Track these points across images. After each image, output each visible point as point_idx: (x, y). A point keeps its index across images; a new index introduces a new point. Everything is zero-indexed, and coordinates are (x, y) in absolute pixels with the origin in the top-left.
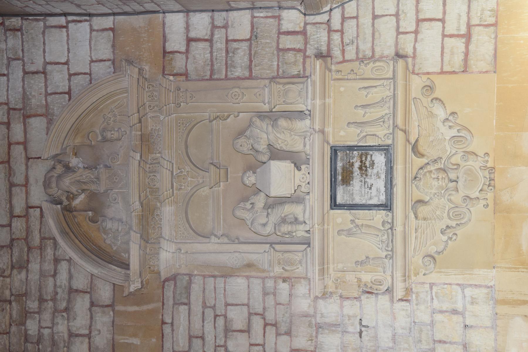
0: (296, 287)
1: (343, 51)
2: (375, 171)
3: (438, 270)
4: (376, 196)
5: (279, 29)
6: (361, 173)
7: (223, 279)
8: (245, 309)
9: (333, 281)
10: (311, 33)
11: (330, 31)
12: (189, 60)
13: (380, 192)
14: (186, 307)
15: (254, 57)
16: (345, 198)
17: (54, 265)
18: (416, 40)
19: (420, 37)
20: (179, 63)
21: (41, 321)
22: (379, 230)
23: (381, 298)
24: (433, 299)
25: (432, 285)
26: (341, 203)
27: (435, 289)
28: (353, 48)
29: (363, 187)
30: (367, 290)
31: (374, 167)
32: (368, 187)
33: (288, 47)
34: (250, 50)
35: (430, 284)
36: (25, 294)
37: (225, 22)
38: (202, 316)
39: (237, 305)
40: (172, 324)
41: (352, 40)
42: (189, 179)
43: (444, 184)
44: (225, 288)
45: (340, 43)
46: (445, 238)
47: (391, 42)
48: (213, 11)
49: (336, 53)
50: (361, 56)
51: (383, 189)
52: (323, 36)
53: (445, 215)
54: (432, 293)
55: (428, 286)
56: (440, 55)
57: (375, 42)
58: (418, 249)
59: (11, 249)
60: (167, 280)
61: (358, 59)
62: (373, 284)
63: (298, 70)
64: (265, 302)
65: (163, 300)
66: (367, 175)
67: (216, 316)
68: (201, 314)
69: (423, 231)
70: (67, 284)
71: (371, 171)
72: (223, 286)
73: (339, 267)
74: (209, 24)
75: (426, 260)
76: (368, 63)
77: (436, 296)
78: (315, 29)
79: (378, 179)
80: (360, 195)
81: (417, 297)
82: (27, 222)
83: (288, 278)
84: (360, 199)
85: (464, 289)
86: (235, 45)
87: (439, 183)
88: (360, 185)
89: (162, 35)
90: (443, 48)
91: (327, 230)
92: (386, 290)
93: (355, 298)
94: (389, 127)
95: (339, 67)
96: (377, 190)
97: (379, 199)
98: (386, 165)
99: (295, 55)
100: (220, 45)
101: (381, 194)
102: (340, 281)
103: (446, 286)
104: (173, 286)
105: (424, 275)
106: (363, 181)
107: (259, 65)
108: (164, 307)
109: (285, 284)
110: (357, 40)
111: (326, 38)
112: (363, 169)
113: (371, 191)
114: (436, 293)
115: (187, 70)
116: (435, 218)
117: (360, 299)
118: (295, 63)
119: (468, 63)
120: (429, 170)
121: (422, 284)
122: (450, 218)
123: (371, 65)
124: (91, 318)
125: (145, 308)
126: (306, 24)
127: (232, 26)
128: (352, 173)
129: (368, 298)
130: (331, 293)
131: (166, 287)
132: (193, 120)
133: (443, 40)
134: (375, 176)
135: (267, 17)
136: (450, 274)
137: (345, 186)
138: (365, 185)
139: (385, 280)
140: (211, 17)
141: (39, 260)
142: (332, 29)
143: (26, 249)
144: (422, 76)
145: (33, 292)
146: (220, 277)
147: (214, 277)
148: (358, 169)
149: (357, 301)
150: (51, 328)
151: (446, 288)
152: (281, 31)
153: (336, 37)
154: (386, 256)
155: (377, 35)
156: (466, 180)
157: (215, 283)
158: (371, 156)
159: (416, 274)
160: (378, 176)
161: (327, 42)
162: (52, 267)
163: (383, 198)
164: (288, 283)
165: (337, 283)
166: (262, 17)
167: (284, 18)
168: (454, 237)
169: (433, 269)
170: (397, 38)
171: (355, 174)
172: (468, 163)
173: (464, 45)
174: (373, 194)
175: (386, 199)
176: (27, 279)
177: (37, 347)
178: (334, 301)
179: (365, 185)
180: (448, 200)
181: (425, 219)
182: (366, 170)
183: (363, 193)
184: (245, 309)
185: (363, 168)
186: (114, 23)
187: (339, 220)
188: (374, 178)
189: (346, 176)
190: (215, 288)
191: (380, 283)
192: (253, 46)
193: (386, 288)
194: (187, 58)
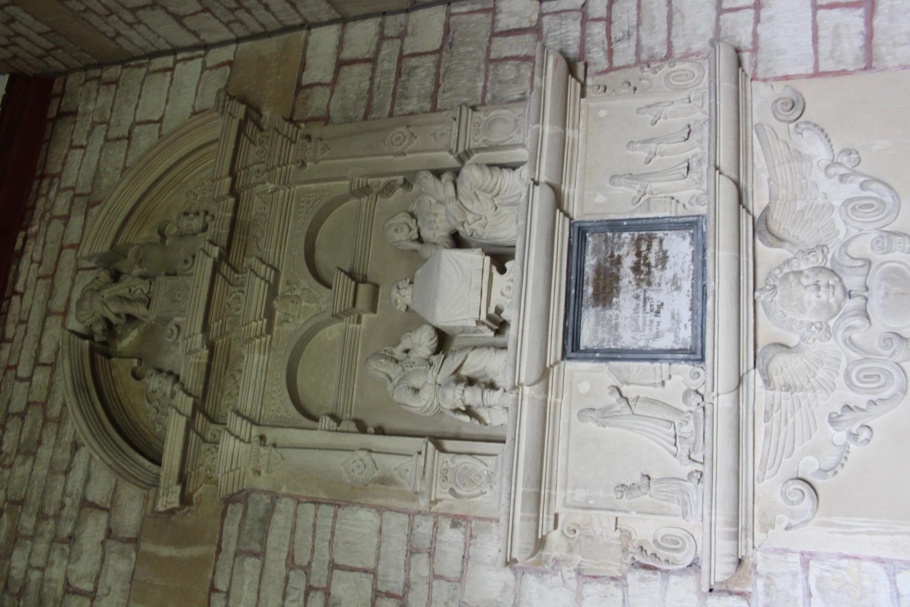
0: (478, 540)
1: (610, 53)
2: (669, 274)
3: (825, 519)
4: (670, 330)
5: (493, 28)
6: (637, 280)
7: (331, 510)
8: (366, 581)
9: (562, 532)
10: (550, 28)
11: (585, 20)
12: (335, 95)
13: (678, 322)
14: (258, 562)
15: (443, 78)
16: (600, 335)
17: (71, 453)
18: (757, 20)
19: (764, 14)
20: (318, 101)
21: (33, 554)
22: (678, 411)
23: (676, 583)
24: (810, 595)
25: (807, 559)
26: (590, 346)
27: (815, 569)
28: (629, 46)
29: (641, 310)
30: (644, 561)
31: (668, 265)
32: (652, 311)
33: (504, 55)
34: (438, 67)
35: (802, 554)
36: (22, 502)
37: (402, 29)
38: (284, 585)
39: (352, 570)
40: (228, 593)
41: (629, 32)
42: (304, 304)
43: (832, 300)
44: (333, 528)
45: (605, 38)
46: (840, 436)
47: (706, 29)
48: (384, 14)
49: (595, 56)
50: (644, 56)
51: (686, 315)
52: (572, 30)
53: (840, 380)
54: (807, 579)
55: (797, 558)
56: (811, 43)
57: (673, 31)
58: (770, 461)
59: (23, 419)
60: (230, 500)
61: (638, 62)
62: (659, 546)
63: (521, 92)
64: (410, 570)
65: (220, 540)
66: (649, 284)
67: (309, 589)
68: (283, 579)
69: (783, 417)
70: (81, 490)
71: (661, 274)
72: (330, 524)
73: (577, 498)
74: (376, 35)
75: (791, 488)
76: (660, 68)
77: (818, 588)
78: (557, 21)
79: (675, 293)
80: (633, 328)
81: (767, 587)
82: (52, 374)
83: (464, 517)
84: (634, 338)
85: (894, 574)
86: (414, 62)
87: (819, 297)
88: (634, 306)
89: (299, 60)
90: (815, 29)
91: (555, 407)
92: (690, 566)
93: (613, 578)
94: (700, 179)
95: (602, 79)
96: (673, 317)
97: (676, 337)
98: (693, 260)
99: (518, 67)
100: (388, 65)
101: (682, 326)
102: (580, 535)
103: (844, 563)
104: (239, 516)
105: (787, 528)
106: (642, 297)
107: (450, 89)
108: (220, 556)
109: (456, 530)
110: (638, 31)
111: (577, 34)
112: (642, 272)
113: (657, 319)
114: (820, 579)
115: (328, 110)
116: (813, 388)
117: (624, 582)
118: (515, 81)
119: (875, 50)
120: (795, 269)
121: (781, 554)
122: (851, 385)
123: (666, 68)
124: (103, 561)
125: (189, 552)
126: (541, 15)
127: (413, 34)
128: (617, 278)
129: (642, 580)
130: (557, 561)
131: (229, 514)
132: (326, 194)
133: (814, 15)
134: (669, 285)
135: (472, 12)
136: (856, 530)
137: (600, 308)
138: (645, 305)
139: (688, 538)
140: (380, 24)
141: (53, 442)
142: (590, 17)
143: (41, 421)
144: (774, 83)
145: (34, 499)
146: (327, 504)
147: (317, 502)
148: (629, 271)
149: (616, 586)
150: (42, 570)
151: (846, 569)
152: (497, 30)
153: (597, 30)
154: (690, 475)
155: (677, 18)
156: (887, 294)
157: (316, 515)
158: (661, 241)
159: (768, 526)
160: (675, 284)
161: (578, 40)
162: (67, 456)
163: (686, 335)
164: (462, 529)
165: (573, 538)
166: (464, 13)
167: (504, 10)
168: (865, 434)
169: (810, 513)
170: (718, 20)
171: (624, 282)
172: (889, 257)
173: (862, 20)
174: (663, 327)
175: (692, 337)
176: (30, 474)
177: (17, 603)
178: (561, 581)
179: (645, 305)
180: (845, 342)
181: (788, 388)
182: (649, 273)
183: (640, 323)
184: (366, 581)
185: (643, 268)
186: (235, 54)
187: (584, 387)
188: (665, 290)
189: (604, 287)
190: (314, 525)
191: (675, 544)
192: (444, 60)
193: (689, 560)
194: (332, 92)
